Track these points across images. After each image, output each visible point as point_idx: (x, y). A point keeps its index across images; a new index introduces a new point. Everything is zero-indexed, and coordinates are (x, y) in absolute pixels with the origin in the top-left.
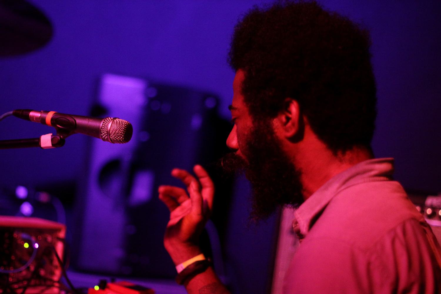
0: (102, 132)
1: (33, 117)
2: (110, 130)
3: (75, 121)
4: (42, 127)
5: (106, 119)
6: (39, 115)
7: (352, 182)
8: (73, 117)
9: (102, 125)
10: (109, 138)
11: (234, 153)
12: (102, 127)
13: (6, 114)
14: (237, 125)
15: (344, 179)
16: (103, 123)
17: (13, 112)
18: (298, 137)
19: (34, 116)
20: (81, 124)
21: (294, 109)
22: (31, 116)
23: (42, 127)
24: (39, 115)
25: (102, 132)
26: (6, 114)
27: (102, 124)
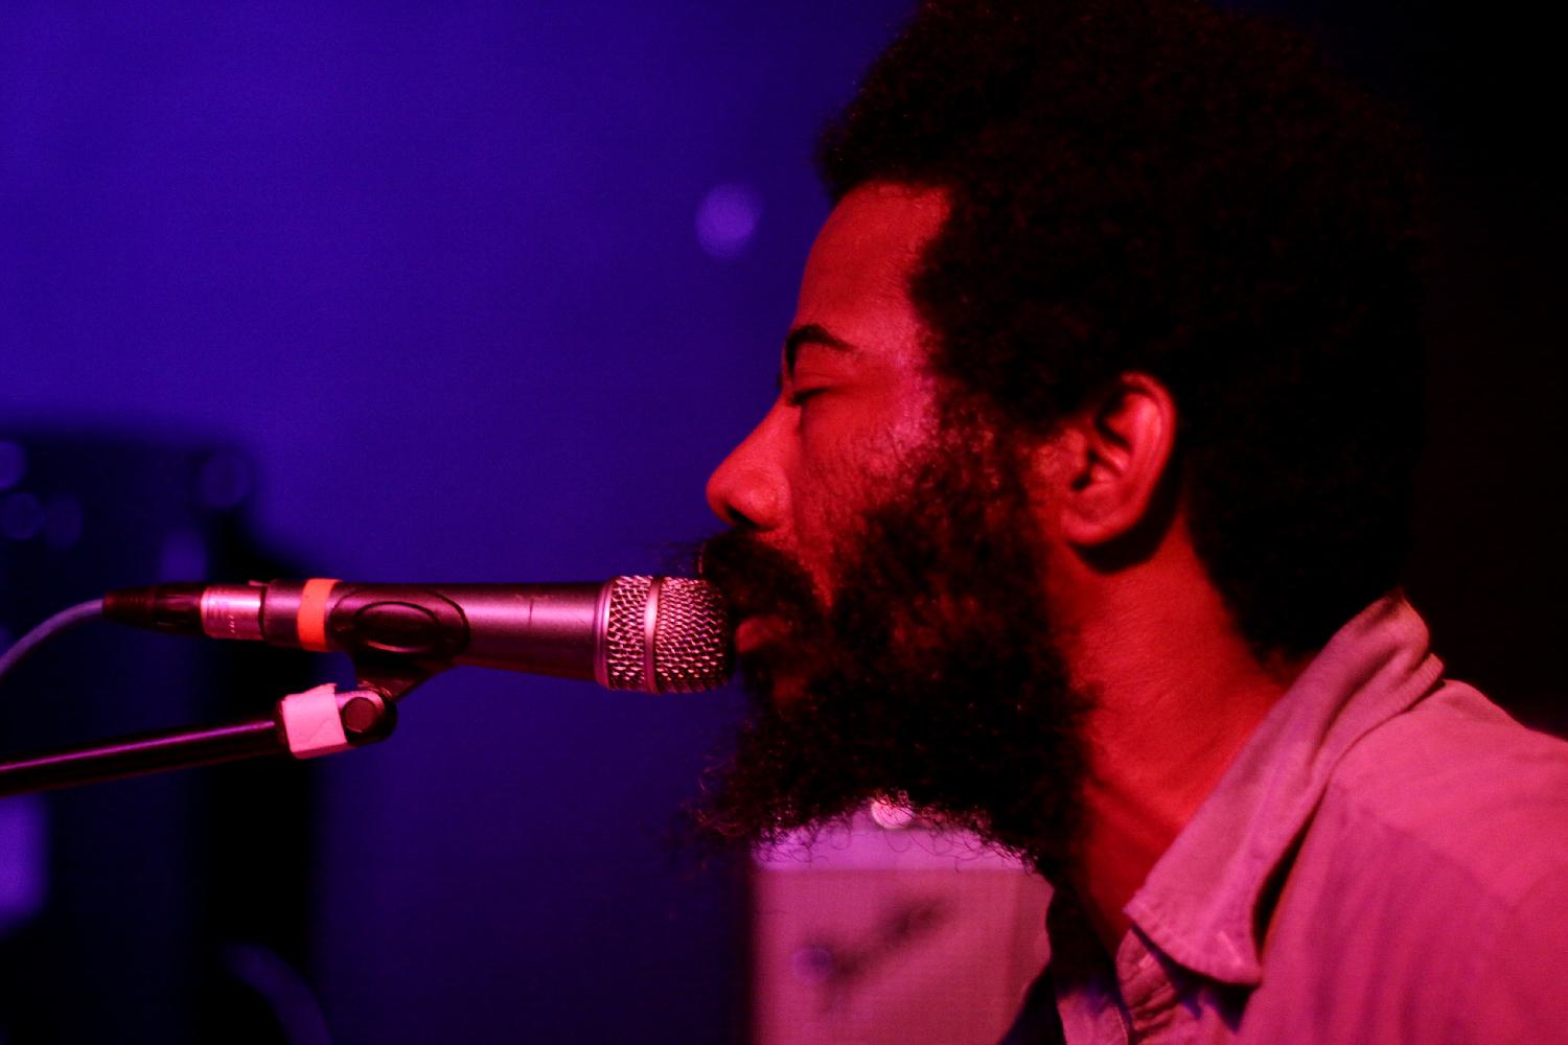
0: (612, 648)
1: (221, 618)
2: (656, 634)
3: (460, 611)
4: (283, 661)
5: (617, 586)
6: (250, 603)
7: (1348, 722)
8: (441, 592)
9: (612, 614)
10: (650, 668)
11: (1023, 852)
12: (611, 625)
13: (63, 617)
14: (912, 826)
15: (1318, 714)
16: (613, 605)
17: (104, 607)
18: (1119, 553)
19: (227, 613)
20: (557, 626)
21: (1150, 419)
22: (210, 614)
23: (283, 661)
24: (250, 603)
25: (612, 648)
26: (63, 617)
27: (607, 614)
